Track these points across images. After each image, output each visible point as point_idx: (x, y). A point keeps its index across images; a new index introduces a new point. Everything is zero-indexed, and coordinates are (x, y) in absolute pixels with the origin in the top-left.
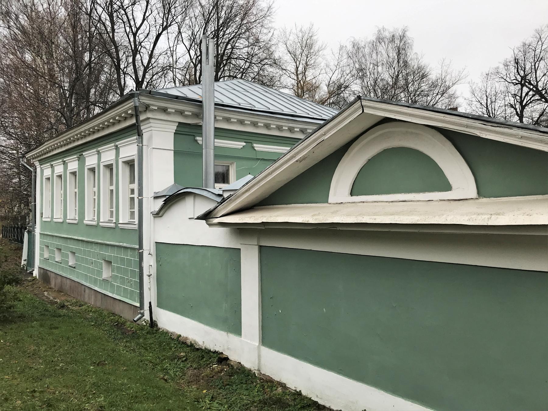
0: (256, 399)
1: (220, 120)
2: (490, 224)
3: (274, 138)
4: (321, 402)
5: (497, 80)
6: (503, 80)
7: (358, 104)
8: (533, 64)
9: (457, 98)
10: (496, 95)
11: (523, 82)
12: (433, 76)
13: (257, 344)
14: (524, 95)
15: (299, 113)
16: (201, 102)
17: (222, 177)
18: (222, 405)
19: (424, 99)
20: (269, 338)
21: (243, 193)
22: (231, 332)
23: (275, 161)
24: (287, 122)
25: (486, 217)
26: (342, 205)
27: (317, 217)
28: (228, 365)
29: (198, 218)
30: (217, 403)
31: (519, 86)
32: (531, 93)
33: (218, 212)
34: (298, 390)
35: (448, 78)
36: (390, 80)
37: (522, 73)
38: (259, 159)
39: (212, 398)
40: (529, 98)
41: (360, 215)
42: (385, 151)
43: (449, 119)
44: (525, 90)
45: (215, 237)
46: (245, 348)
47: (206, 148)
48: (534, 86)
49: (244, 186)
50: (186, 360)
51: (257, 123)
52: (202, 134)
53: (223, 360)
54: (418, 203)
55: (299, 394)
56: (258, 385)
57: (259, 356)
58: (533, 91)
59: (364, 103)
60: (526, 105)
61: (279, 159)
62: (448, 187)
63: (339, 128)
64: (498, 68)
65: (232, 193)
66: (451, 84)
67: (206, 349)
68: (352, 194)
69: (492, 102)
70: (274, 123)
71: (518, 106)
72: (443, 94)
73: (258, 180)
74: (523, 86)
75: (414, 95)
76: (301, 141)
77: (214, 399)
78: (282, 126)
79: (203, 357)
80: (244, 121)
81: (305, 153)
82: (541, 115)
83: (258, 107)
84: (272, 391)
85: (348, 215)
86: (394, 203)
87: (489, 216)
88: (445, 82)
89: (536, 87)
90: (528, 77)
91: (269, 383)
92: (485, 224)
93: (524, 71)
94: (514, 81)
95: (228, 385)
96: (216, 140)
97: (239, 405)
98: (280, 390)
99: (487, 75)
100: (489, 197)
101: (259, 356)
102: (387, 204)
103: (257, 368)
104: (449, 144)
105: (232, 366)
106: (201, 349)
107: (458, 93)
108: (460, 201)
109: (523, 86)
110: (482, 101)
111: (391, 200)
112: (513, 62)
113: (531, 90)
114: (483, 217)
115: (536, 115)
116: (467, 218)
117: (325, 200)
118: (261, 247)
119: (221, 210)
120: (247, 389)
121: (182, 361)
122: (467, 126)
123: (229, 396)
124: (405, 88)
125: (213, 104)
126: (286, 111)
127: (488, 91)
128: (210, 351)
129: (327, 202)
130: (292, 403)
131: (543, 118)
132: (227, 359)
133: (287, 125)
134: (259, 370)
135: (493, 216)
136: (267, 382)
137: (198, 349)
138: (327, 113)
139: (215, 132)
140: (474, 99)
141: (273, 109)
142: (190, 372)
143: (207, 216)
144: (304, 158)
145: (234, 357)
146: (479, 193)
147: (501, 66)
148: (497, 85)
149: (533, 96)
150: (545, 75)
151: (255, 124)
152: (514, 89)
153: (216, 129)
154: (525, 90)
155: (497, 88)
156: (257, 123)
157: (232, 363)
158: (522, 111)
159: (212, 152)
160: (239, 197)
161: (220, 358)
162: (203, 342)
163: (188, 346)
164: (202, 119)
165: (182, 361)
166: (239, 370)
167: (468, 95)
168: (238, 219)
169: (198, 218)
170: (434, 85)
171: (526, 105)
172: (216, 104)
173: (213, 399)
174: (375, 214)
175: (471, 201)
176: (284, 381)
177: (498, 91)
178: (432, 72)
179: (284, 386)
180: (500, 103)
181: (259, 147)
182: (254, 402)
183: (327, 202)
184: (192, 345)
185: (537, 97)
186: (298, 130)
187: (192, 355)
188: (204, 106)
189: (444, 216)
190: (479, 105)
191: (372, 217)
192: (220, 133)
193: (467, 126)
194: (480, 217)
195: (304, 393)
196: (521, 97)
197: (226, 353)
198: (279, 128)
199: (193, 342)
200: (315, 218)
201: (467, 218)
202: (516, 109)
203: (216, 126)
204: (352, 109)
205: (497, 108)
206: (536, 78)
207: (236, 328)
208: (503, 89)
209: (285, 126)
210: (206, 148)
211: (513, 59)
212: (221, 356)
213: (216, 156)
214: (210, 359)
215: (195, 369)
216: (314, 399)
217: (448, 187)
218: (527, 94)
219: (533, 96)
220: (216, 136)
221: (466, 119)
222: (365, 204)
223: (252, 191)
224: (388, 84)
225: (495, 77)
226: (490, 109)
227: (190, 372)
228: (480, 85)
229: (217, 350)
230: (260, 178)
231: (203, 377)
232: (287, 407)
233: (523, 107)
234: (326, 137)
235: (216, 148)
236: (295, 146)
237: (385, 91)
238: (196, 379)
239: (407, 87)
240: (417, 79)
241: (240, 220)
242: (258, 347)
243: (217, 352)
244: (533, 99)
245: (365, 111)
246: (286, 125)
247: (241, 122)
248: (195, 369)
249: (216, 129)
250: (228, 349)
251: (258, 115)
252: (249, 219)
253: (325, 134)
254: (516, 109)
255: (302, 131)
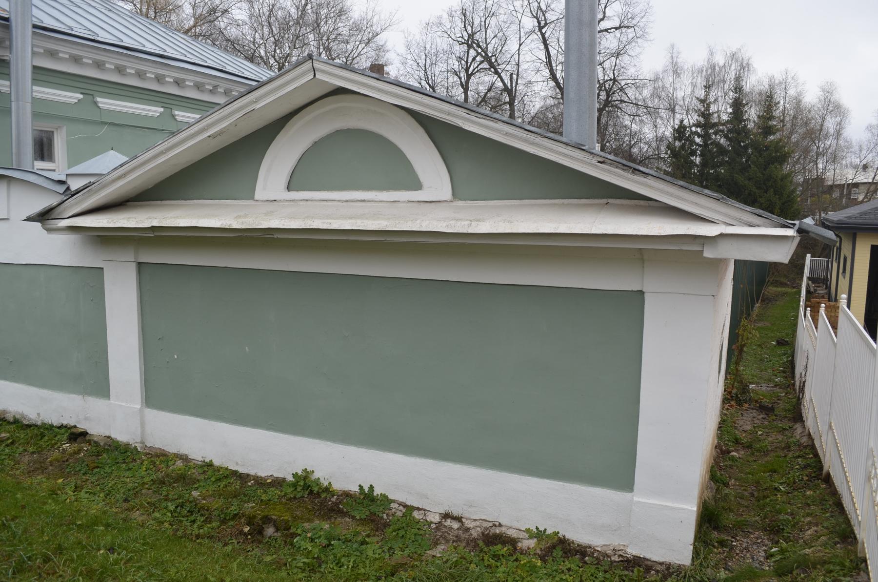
0: (146, 480)
1: (88, 64)
2: (470, 231)
3: (78, 79)
4: (242, 470)
5: (439, 33)
6: (446, 35)
7: (308, 65)
8: (483, 19)
9: (388, 51)
10: (436, 55)
11: (470, 42)
12: (356, 13)
13: (139, 406)
14: (470, 59)
15: (170, 52)
16: (7, 19)
17: (43, 149)
18: (95, 494)
19: (343, 46)
20: (153, 397)
21: (114, 181)
22: (90, 394)
23: (173, 134)
24: (154, 65)
25: (466, 223)
26: (275, 203)
27: (244, 220)
28: (89, 442)
29: (29, 219)
30: (86, 493)
31: (465, 47)
32: (479, 58)
33: (65, 210)
34: (207, 460)
35: (375, 20)
36: (293, 10)
37: (469, 29)
38: (106, 123)
39: (76, 487)
40: (476, 65)
41: (308, 217)
42: (338, 132)
43: (428, 102)
44: (472, 53)
45: (54, 249)
46: (120, 413)
47: (17, 100)
48: (483, 50)
49: (116, 169)
50: (12, 443)
51: (104, 63)
52: (9, 75)
53: (77, 436)
54: (380, 204)
55: (210, 465)
56: (146, 462)
57: (143, 424)
58: (482, 56)
59: (317, 65)
60: (472, 74)
61: (179, 132)
62: (417, 185)
63: (278, 96)
64: (441, 17)
65: (92, 180)
66: (379, 29)
67: (44, 424)
68: (289, 188)
69: (432, 64)
70: (132, 67)
71: (463, 75)
72: (368, 43)
73: (141, 161)
74: (470, 47)
75: (328, 39)
76: (218, 107)
77: (79, 489)
78: (145, 72)
79: (43, 436)
80: (81, 57)
81: (223, 126)
82: (489, 90)
83: (103, 36)
84: (168, 467)
85: (291, 217)
86: (349, 203)
87: (469, 223)
88: (372, 26)
89: (485, 50)
90: (477, 37)
91: (160, 457)
92: (634, 233)
93: (472, 27)
94: (460, 39)
95: (98, 467)
96: (35, 88)
97: (122, 491)
98: (179, 464)
99: (428, 24)
100: (465, 200)
101: (143, 424)
102: (340, 203)
103: (139, 441)
104: (421, 131)
105: (95, 442)
106: (36, 426)
107: (389, 46)
108: (430, 202)
109: (470, 47)
110: (419, 61)
111: (345, 199)
112: (459, 13)
113: (478, 54)
114: (463, 223)
115: (483, 89)
116: (445, 224)
117: (250, 195)
118: (140, 264)
119: (72, 206)
120: (129, 469)
121: (7, 445)
122: (449, 114)
123: (102, 481)
124: (317, 25)
125: (30, 27)
126: (149, 47)
127: (428, 47)
128: (52, 426)
129: (253, 198)
130: (202, 477)
131: (490, 95)
132: (84, 434)
133: (153, 70)
134: (142, 443)
135: (473, 223)
136: (157, 456)
137: (29, 426)
138: (263, 74)
139: (33, 73)
140: (409, 57)
141: (127, 42)
142: (26, 459)
143: (44, 217)
144: (220, 133)
145: (96, 430)
146: (454, 194)
147: (445, 16)
148: (439, 40)
149: (481, 62)
150: (495, 36)
151: (99, 65)
152: (460, 50)
153: (35, 68)
154: (472, 53)
155: (439, 45)
156: (104, 63)
157: (95, 439)
158: (467, 82)
159: (28, 107)
160: (104, 186)
161: (72, 434)
162: (38, 414)
163: (9, 423)
164: (10, 48)
165: (7, 445)
166: (110, 446)
167: (402, 50)
168: (105, 221)
169: (29, 219)
170: (357, 28)
171: (472, 74)
172: (35, 26)
173: (77, 488)
174: (328, 217)
175: (445, 204)
176: (183, 451)
177: (440, 49)
178: (355, 8)
179: (185, 458)
180: (441, 67)
181: (105, 103)
182: (144, 484)
183: (253, 198)
184: (16, 421)
185: (485, 65)
186: (133, 72)
187: (22, 435)
188: (14, 28)
189: (418, 221)
190: (415, 66)
191: (327, 221)
192: (41, 75)
193: (449, 114)
194: (459, 223)
195: (217, 463)
196: (467, 62)
197: (82, 426)
198: (140, 75)
199: (18, 416)
200: (240, 220)
201: (445, 224)
202: (460, 78)
203: (35, 64)
204: (299, 70)
205: (437, 73)
206: (486, 38)
207: (98, 384)
208: (446, 48)
209: (151, 73)
210: (17, 100)
211: (459, 8)
212: (73, 430)
213: (35, 115)
214: (55, 436)
215: (33, 453)
216: (233, 467)
217: (417, 185)
218: (474, 59)
219: (481, 62)
220: (35, 81)
221: (448, 105)
222: (309, 203)
223: (130, 179)
224: (290, 16)
225: (436, 29)
226: (429, 73)
227: (26, 459)
228: (418, 37)
229: (65, 423)
230: (146, 158)
231: (51, 462)
232: (195, 483)
233: (469, 76)
234: (258, 106)
235: (35, 100)
236: (208, 113)
237: (285, 27)
238: (40, 467)
239: (318, 26)
240: (332, 15)
241: (108, 222)
242: (141, 410)
243: (66, 427)
244: (480, 67)
245: (317, 76)
246: (152, 72)
247: (76, 60)
248: (33, 453)
249: (35, 68)
250: (86, 419)
251: (121, 54)
252: (125, 221)
253: (257, 101)
254: (460, 78)
255: (226, 93)
